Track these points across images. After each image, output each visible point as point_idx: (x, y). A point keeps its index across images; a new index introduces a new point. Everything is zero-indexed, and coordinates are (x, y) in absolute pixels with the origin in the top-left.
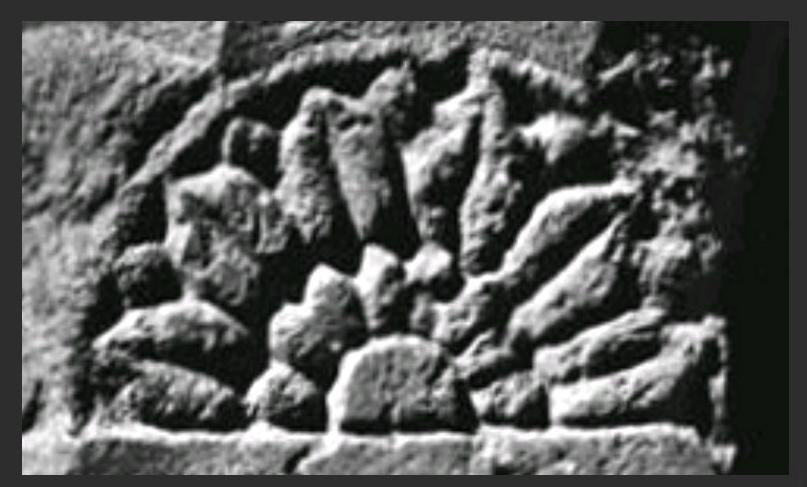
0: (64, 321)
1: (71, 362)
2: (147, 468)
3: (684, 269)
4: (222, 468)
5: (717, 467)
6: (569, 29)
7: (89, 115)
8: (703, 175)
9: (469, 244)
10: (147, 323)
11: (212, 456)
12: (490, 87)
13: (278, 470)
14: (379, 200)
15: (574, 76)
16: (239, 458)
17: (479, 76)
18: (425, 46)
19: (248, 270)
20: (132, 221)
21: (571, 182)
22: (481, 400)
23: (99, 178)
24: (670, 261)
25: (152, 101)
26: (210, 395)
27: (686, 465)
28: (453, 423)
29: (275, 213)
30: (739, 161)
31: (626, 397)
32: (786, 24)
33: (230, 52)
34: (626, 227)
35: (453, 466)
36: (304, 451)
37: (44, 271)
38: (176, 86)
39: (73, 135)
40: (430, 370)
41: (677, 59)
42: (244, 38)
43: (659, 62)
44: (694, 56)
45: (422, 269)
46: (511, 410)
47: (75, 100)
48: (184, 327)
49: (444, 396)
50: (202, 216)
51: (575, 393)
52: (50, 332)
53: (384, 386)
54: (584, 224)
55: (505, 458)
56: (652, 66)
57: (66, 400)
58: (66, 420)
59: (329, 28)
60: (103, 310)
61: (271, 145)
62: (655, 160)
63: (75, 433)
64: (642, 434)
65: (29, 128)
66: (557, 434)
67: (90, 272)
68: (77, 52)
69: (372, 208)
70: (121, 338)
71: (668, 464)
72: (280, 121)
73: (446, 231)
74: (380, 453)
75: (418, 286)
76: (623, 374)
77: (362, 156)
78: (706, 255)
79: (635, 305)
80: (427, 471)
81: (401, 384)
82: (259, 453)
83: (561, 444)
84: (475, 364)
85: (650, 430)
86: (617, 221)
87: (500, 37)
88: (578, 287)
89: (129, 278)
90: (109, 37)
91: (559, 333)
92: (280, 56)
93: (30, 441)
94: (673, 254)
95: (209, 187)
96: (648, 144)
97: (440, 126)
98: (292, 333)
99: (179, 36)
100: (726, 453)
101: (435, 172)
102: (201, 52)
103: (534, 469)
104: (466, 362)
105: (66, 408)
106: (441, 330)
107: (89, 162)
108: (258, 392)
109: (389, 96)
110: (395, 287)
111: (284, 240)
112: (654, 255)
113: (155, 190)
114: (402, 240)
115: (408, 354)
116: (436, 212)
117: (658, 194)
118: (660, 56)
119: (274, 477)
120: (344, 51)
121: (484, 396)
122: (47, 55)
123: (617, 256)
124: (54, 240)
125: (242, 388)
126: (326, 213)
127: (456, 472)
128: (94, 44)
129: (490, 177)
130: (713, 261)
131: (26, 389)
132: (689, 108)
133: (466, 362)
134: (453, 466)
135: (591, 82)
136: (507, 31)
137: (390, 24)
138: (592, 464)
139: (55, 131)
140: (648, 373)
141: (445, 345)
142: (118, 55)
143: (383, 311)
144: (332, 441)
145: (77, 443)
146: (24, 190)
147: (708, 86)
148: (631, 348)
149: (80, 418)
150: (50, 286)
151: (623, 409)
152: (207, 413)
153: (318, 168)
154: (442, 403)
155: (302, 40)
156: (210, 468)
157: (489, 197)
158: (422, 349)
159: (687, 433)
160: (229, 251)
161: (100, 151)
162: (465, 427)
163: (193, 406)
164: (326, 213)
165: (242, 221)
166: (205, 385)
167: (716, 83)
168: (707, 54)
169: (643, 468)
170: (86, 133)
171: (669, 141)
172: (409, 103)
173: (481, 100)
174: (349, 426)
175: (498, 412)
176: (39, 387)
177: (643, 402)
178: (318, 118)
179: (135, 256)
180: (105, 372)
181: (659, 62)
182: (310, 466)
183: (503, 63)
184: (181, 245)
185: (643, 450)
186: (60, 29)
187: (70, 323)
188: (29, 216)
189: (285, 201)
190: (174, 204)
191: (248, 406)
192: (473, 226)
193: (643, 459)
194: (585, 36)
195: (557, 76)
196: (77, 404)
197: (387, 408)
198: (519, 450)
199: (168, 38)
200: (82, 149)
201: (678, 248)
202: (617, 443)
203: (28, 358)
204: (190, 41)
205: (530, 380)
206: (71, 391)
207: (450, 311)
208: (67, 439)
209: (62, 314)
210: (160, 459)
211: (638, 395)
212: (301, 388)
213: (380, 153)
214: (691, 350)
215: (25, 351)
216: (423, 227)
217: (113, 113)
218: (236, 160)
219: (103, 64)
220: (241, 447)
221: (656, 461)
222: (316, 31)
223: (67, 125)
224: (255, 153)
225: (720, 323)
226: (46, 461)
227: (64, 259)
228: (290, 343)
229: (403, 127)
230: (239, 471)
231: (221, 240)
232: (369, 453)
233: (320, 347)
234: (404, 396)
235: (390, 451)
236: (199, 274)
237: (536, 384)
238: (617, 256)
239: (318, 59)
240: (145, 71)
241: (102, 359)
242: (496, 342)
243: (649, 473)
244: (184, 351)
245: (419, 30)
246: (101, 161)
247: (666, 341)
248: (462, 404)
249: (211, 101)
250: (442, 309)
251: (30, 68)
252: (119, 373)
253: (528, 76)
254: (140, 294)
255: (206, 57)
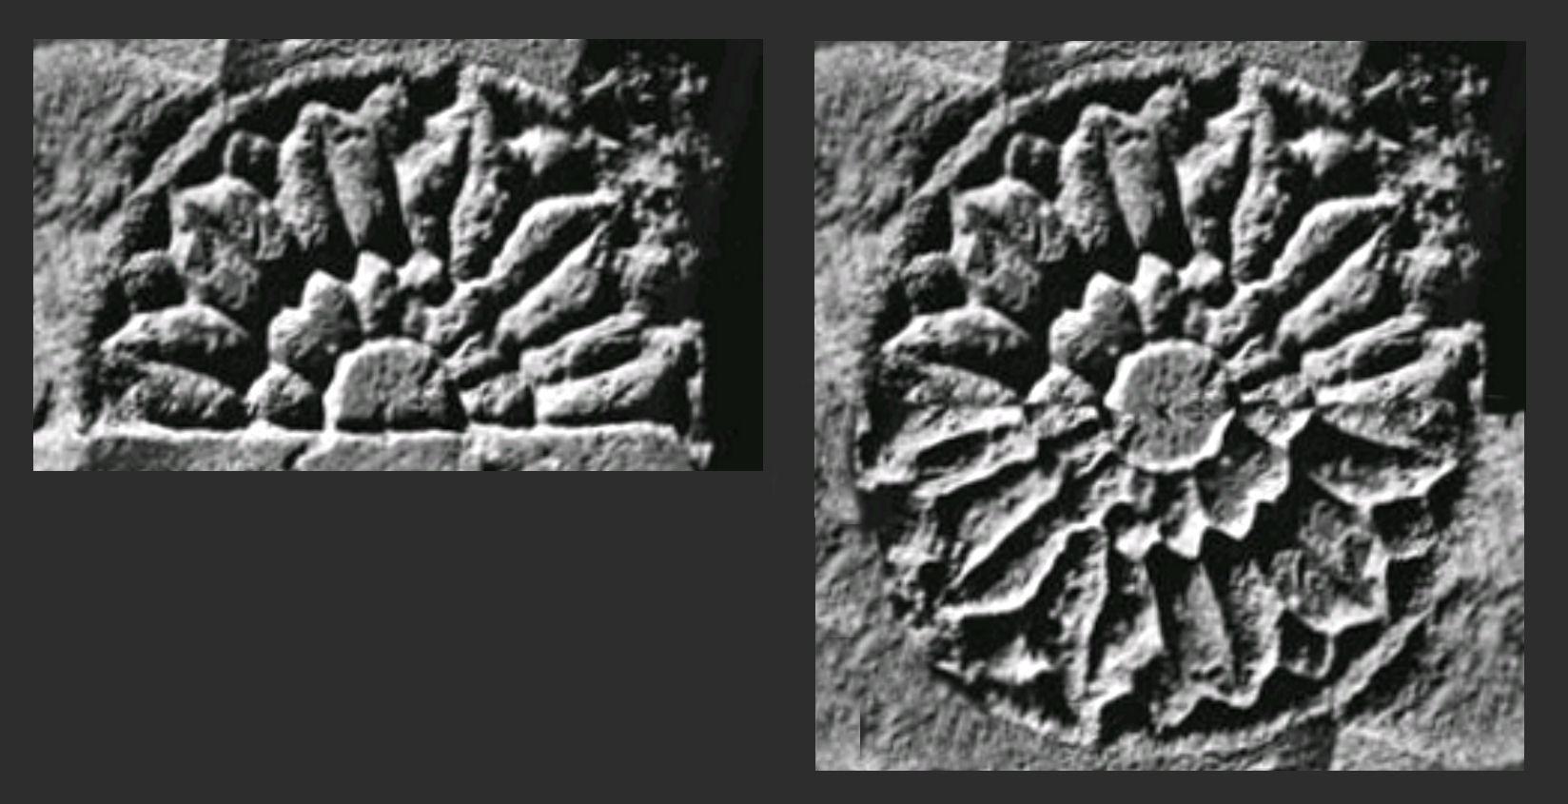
0: (855, 327)
1: (861, 365)
2: (152, 465)
3: (663, 275)
4: (223, 464)
5: (695, 464)
6: (1335, 49)
7: (878, 131)
8: (681, 186)
9: (1240, 254)
10: (152, 327)
11: (214, 453)
12: (1260, 104)
13: (276, 466)
14: (373, 209)
15: (558, 91)
16: (240, 454)
17: (468, 91)
18: (1198, 64)
19: (248, 276)
20: (138, 230)
21: (1336, 194)
22: (470, 400)
23: (106, 188)
24: (1431, 269)
25: (157, 115)
26: (212, 395)
27: (665, 461)
28: (443, 421)
29: (1055, 223)
30: (716, 172)
31: (608, 397)
32: (760, 43)
33: (231, 68)
34: (1389, 237)
35: (443, 463)
36: (302, 448)
37: (54, 277)
38: (961, 103)
39: (863, 149)
40: (422, 371)
41: (656, 75)
42: (245, 55)
43: (1420, 79)
44: (673, 72)
45: (414, 275)
46: (498, 409)
47: (84, 114)
48: (187, 330)
49: (434, 396)
50: (204, 225)
51: (559, 393)
52: (60, 335)
53: (378, 386)
54: (1350, 234)
55: (493, 455)
56: (633, 82)
57: (75, 399)
58: (75, 418)
59: (1107, 48)
60: (111, 314)
61: (1051, 159)
62: (1417, 173)
63: (84, 431)
64: (622, 432)
65: (39, 141)
66: (542, 432)
67: (880, 280)
68: (85, 70)
69: (366, 217)
70: (128, 341)
71: (648, 461)
72: (279, 134)
73: (437, 239)
74: (374, 450)
75: (1191, 293)
76: (605, 375)
77: (356, 168)
78: (684, 262)
79: (1397, 311)
80: (419, 467)
81: (1176, 386)
82: (259, 450)
83: (546, 441)
84: (464, 365)
85: (631, 428)
86: (600, 229)
87: (488, 55)
88: (562, 292)
89: (135, 284)
90: (116, 54)
91: (544, 336)
92: (1060, 74)
93: (41, 439)
94: (653, 261)
95: (211, 197)
96: (1410, 158)
97: (1212, 141)
98: (290, 336)
99: (964, 55)
100: (703, 450)
101: (1207, 184)
102: (985, 70)
103: (521, 466)
104: (456, 363)
105: (75, 407)
106: (1213, 335)
107: (97, 173)
108: (258, 392)
109: (1164, 112)
110: (388, 292)
111: (1063, 250)
112: (635, 261)
113: (941, 201)
114: (394, 246)
115: (400, 356)
116: (427, 221)
117: (1419, 205)
118: (640, 72)
119: (273, 473)
120: (340, 67)
121: (473, 396)
122: (838, 73)
123: (1380, 265)
124: (844, 249)
125: (243, 388)
126: (322, 222)
127: (446, 468)
128: (883, 63)
129: (1260, 189)
130: (1472, 269)
131: (37, 390)
132: (668, 121)
133: (456, 363)
134: (443, 463)
135: (575, 97)
136: (495, 48)
137: (383, 42)
138: (576, 460)
139: (64, 143)
140: (629, 374)
141: (1217, 349)
142: (906, 74)
143: (1158, 317)
144: (328, 439)
145: (86, 440)
146: (816, 202)
147: (1467, 102)
148: (612, 351)
149: (89, 417)
150: (60, 291)
151: (605, 409)
152: (209, 412)
153: (315, 179)
154: (433, 403)
155: (1081, 59)
156: (212, 465)
157: (1259, 208)
158: (413, 351)
159: (666, 431)
160: (230, 258)
161: (107, 163)
162: (454, 425)
163: (196, 405)
164: (322, 222)
165: (1024, 231)
166: (207, 386)
167: (1475, 100)
168: (1466, 72)
169: (624, 465)
170: (94, 146)
171: (649, 153)
172: (402, 117)
173: (1251, 116)
174: (344, 425)
175: (486, 411)
176: (49, 387)
177: (624, 402)
178: (315, 131)
179: (141, 263)
180: (113, 373)
181: (1420, 79)
182: (308, 463)
183: (491, 79)
184: (185, 252)
185: (624, 447)
186: (850, 49)
187: (860, 329)
188: (40, 224)
189: (283, 210)
190: (959, 215)
191: (248, 405)
192: (462, 235)
193: (624, 456)
194: (1350, 55)
195: (1324, 93)
196: (86, 404)
197: (381, 407)
198: (507, 448)
199: (172, 55)
200: (871, 162)
201: (1441, 257)
202: (599, 441)
203: (39, 359)
204: (193, 58)
205: (1298, 383)
206: (80, 391)
207: (441, 315)
208: (76, 437)
209: (852, 320)
210: (165, 456)
211: (620, 394)
212: (299, 389)
213: (374, 165)
214: (670, 352)
215: (36, 353)
216: (1196, 237)
217: (120, 127)
218: (237, 171)
219: (111, 80)
220: (242, 445)
221: (637, 458)
222: (314, 48)
223: (857, 140)
224: (254, 165)
225: (698, 326)
226: (56, 458)
227: (73, 266)
228: (1069, 347)
229: (1177, 142)
230: (240, 467)
231: (1003, 249)
232: (363, 450)
233: (1098, 352)
234: (397, 396)
235: (384, 449)
236: (983, 282)
237: (522, 385)
238: (1380, 265)
239: (1097, 77)
240: (150, 86)
241: (109, 361)
242: (1265, 346)
243: (630, 469)
244: (188, 353)
245: (1192, 49)
246: (108, 172)
247: (646, 344)
248: (452, 404)
249: (213, 115)
250: (433, 313)
251: (41, 84)
252: (126, 374)
253: (1296, 94)
254: (146, 299)
255: (208, 74)
